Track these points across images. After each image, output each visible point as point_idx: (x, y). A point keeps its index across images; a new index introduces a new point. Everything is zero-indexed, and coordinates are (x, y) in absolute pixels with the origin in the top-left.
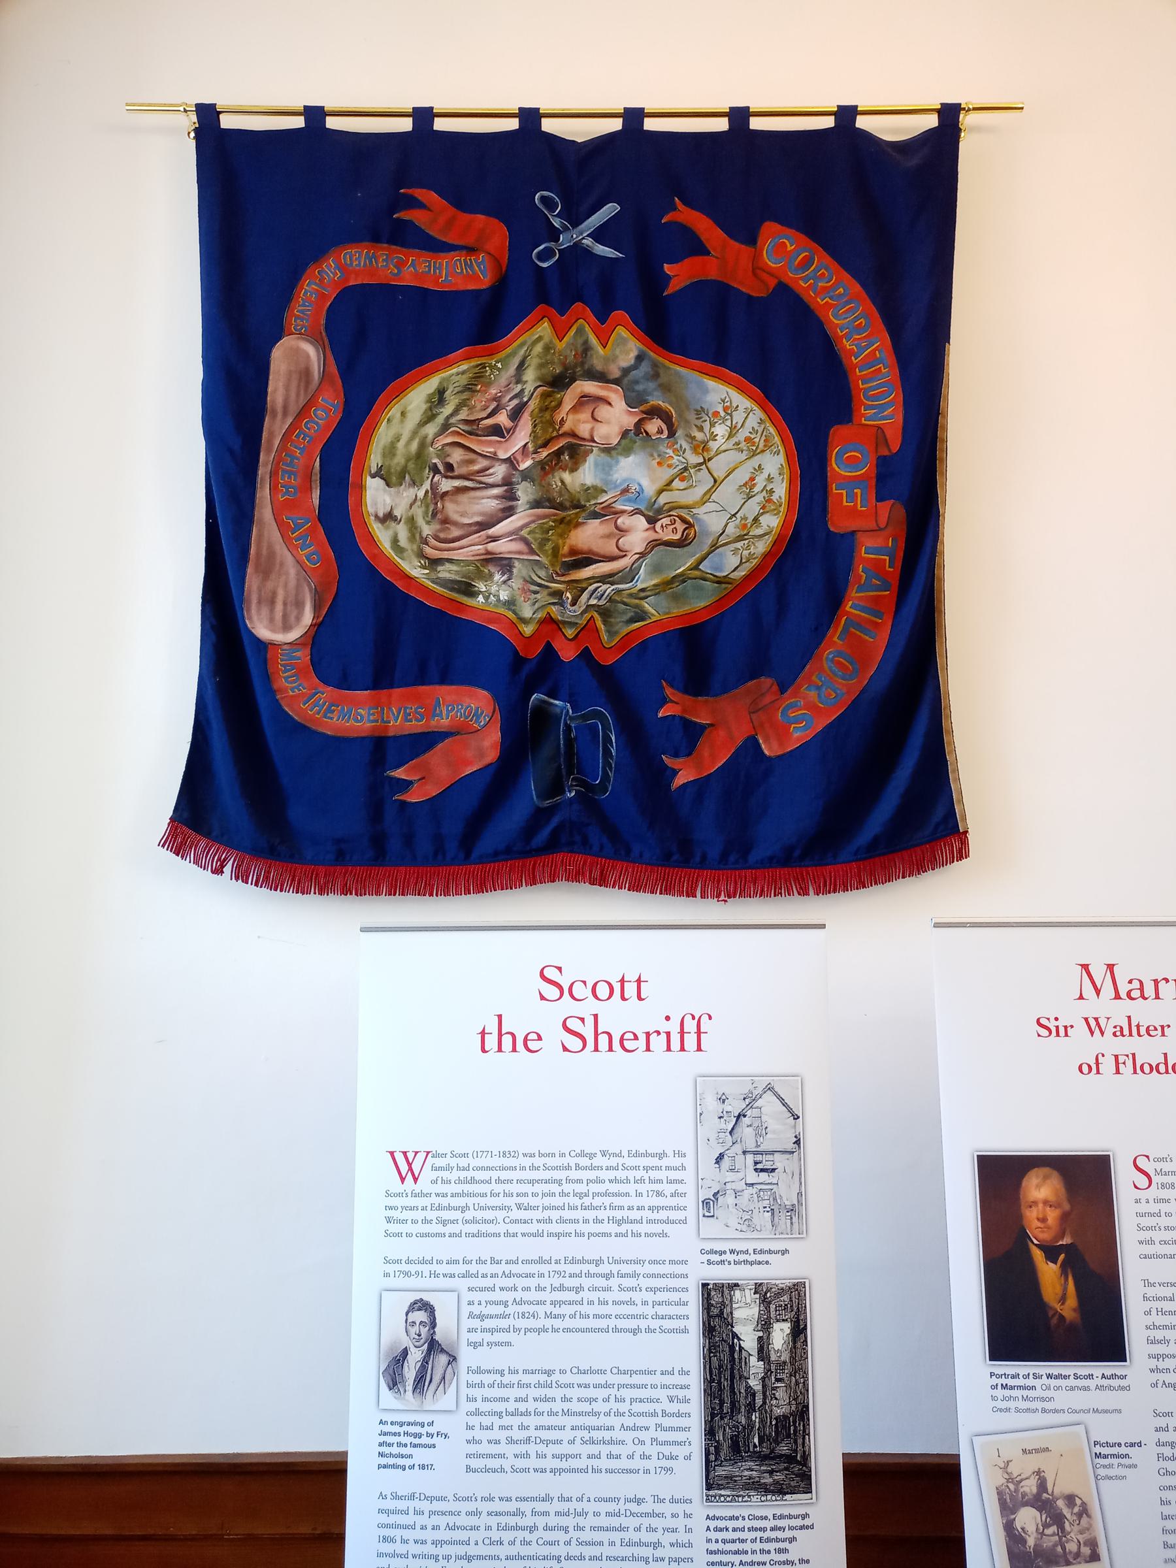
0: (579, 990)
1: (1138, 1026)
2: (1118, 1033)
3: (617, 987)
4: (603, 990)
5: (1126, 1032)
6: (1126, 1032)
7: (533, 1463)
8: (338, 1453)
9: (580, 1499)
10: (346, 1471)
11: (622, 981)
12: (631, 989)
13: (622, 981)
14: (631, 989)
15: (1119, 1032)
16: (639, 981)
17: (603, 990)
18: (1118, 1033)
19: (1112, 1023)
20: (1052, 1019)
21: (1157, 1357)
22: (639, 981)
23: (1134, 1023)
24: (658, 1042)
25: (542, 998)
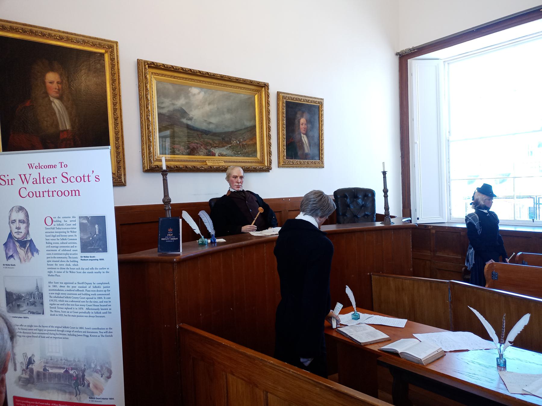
0: (72, 179)
1: (43, 178)
2: (35, 182)
3: (82, 178)
4: (79, 179)
5: (38, 182)
6: (38, 182)
7: (71, 285)
8: (318, 145)
9: (21, 325)
10: (118, 254)
11: (84, 176)
12: (86, 178)
13: (84, 176)
14: (86, 178)
15: (35, 182)
16: (88, 176)
17: (79, 179)
18: (35, 182)
19: (32, 177)
20: (6, 176)
21: (52, 305)
22: (88, 176)
23: (41, 177)
24: (46, 194)
25: (63, 182)
